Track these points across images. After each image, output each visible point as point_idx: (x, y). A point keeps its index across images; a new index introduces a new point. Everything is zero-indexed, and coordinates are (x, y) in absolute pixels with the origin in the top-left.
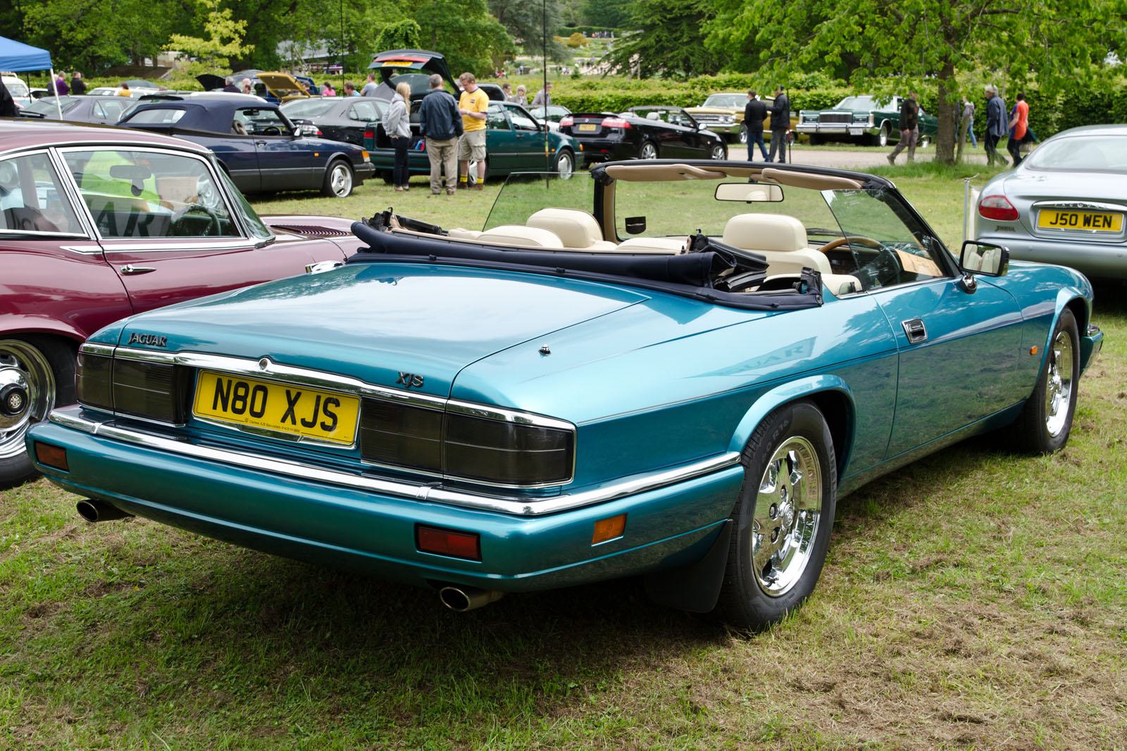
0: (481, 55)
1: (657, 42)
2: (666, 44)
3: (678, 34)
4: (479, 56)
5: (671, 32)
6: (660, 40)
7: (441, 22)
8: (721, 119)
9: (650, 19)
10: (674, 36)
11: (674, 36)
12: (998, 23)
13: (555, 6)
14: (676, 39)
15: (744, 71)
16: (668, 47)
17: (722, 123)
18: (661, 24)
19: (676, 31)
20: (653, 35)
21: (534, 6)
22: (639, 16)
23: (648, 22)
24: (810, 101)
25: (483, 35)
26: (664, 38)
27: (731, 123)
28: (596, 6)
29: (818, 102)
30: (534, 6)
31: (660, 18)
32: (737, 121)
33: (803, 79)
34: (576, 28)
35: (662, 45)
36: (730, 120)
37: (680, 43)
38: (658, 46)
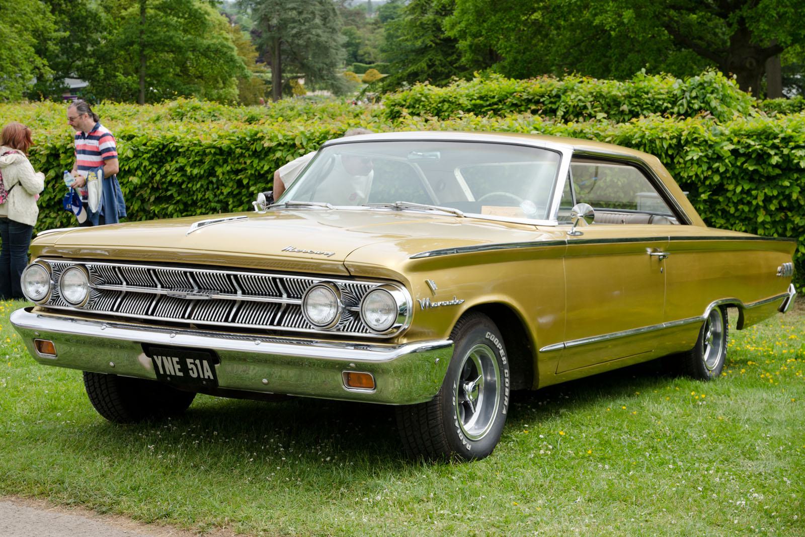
0: (224, 83)
1: (429, 67)
2: (440, 69)
3: (455, 57)
4: (222, 85)
5: (446, 55)
6: (434, 65)
7: (150, 39)
8: (321, 309)
9: (421, 40)
10: (449, 59)
11: (449, 59)
12: (36, 272)
13: (335, 37)
14: (451, 63)
15: (520, 77)
16: (442, 73)
17: (329, 337)
18: (434, 45)
19: (453, 53)
20: (426, 59)
21: (311, 36)
22: (409, 37)
23: (419, 43)
24: (734, 152)
25: (206, 56)
26: (437, 63)
27: (387, 340)
28: (391, 44)
29: (762, 157)
30: (311, 36)
31: (433, 38)
32: (423, 319)
33: (677, 92)
34: (372, 65)
35: (435, 71)
36: (376, 318)
37: (456, 68)
38: (430, 72)
